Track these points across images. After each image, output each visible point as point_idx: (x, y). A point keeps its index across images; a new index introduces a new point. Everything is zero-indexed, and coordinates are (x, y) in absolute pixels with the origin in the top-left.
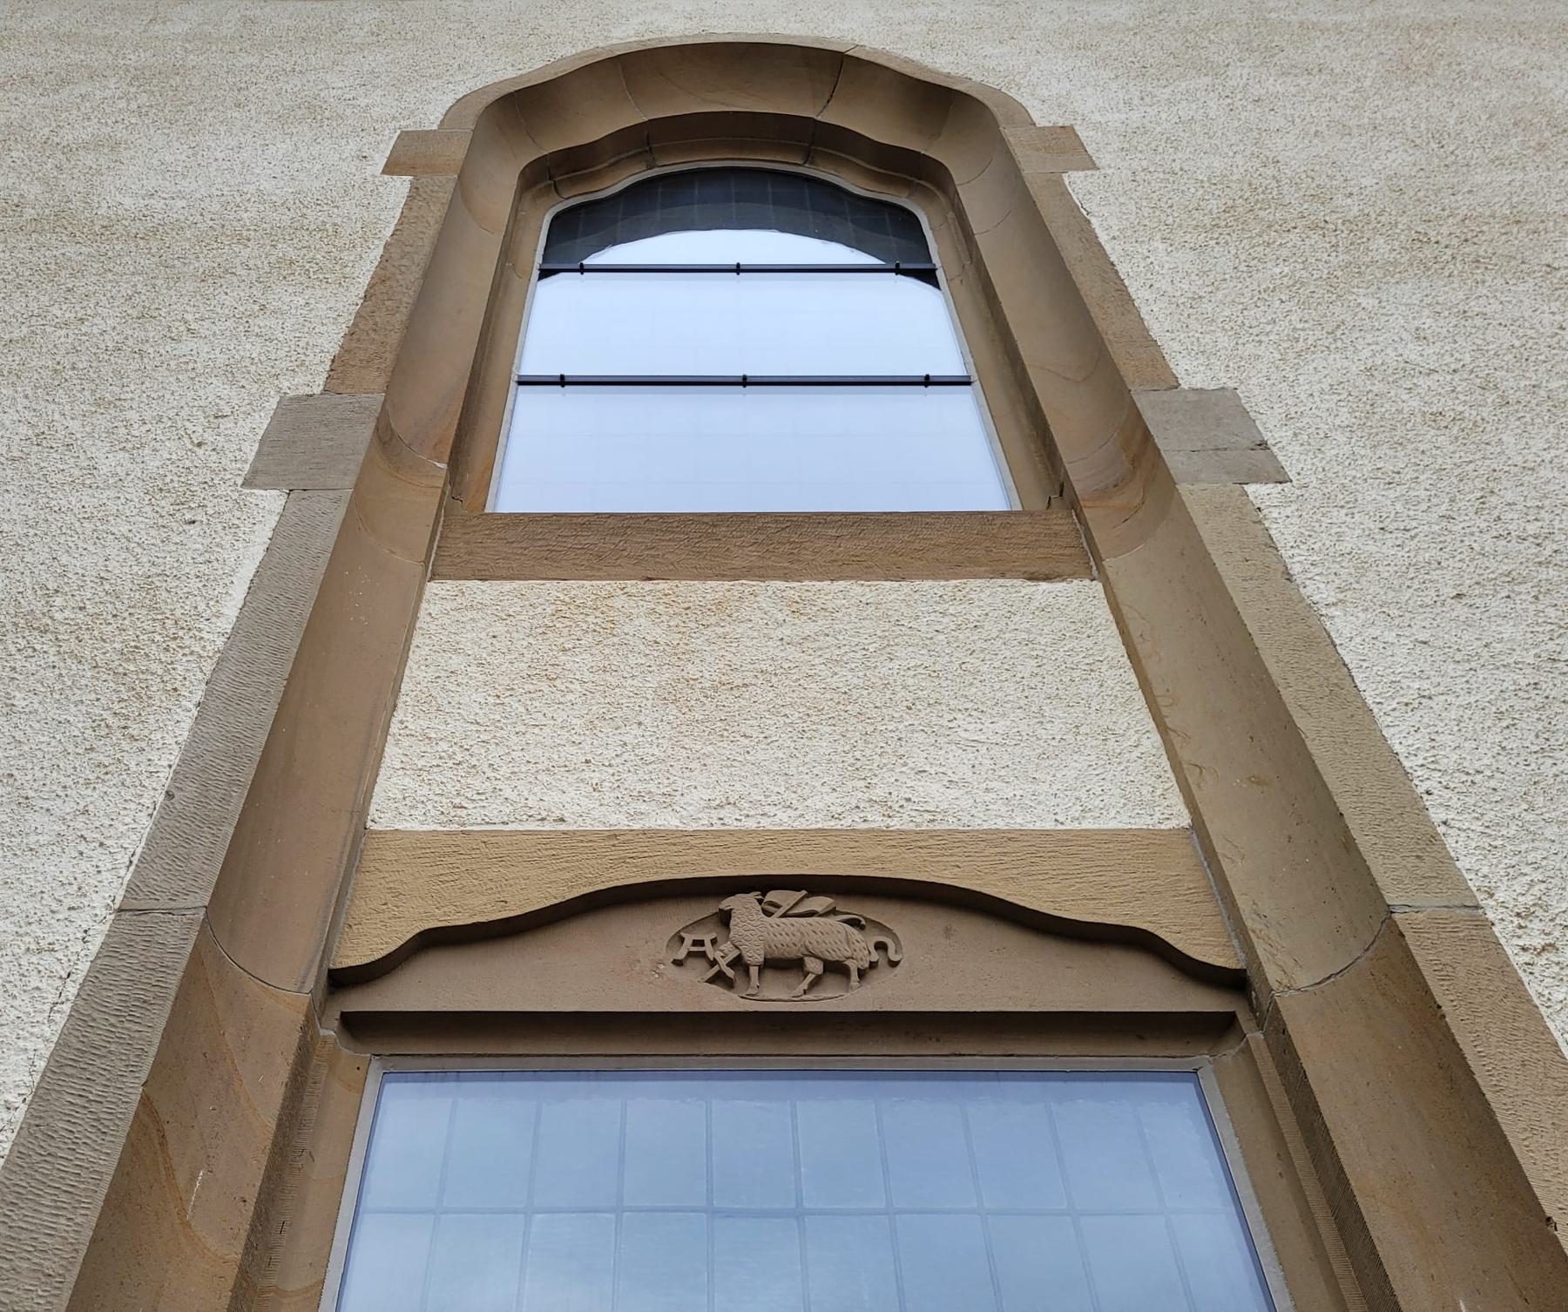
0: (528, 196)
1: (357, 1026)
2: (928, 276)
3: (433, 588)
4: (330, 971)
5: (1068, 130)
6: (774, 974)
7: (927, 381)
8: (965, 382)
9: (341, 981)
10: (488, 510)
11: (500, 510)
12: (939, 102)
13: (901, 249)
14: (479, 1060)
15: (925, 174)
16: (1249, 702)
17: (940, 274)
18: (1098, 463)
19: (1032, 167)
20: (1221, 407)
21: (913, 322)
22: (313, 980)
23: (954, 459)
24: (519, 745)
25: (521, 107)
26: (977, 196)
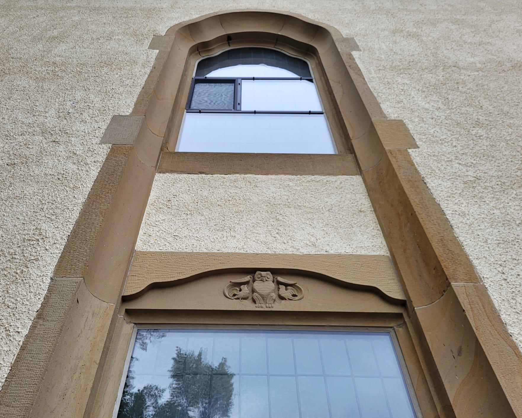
0: (191, 56)
1: (129, 312)
2: (311, 81)
3: (158, 177)
4: (123, 296)
5: (401, 121)
6: (272, 298)
7: (310, 113)
8: (322, 113)
9: (125, 299)
10: (170, 150)
11: (180, 151)
12: (317, 31)
13: (302, 70)
14: (346, 328)
15: (311, 51)
16: (401, 209)
17: (314, 80)
18: (362, 141)
19: (340, 47)
20: (399, 126)
21: (305, 94)
22: (116, 299)
23: (317, 137)
24: (181, 224)
25: (191, 28)
26: (322, 50)
